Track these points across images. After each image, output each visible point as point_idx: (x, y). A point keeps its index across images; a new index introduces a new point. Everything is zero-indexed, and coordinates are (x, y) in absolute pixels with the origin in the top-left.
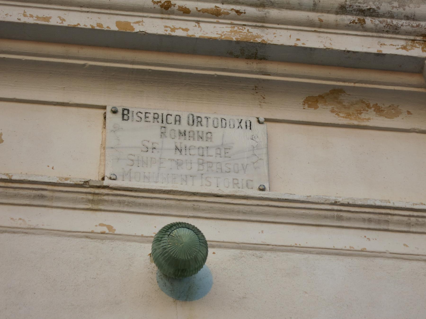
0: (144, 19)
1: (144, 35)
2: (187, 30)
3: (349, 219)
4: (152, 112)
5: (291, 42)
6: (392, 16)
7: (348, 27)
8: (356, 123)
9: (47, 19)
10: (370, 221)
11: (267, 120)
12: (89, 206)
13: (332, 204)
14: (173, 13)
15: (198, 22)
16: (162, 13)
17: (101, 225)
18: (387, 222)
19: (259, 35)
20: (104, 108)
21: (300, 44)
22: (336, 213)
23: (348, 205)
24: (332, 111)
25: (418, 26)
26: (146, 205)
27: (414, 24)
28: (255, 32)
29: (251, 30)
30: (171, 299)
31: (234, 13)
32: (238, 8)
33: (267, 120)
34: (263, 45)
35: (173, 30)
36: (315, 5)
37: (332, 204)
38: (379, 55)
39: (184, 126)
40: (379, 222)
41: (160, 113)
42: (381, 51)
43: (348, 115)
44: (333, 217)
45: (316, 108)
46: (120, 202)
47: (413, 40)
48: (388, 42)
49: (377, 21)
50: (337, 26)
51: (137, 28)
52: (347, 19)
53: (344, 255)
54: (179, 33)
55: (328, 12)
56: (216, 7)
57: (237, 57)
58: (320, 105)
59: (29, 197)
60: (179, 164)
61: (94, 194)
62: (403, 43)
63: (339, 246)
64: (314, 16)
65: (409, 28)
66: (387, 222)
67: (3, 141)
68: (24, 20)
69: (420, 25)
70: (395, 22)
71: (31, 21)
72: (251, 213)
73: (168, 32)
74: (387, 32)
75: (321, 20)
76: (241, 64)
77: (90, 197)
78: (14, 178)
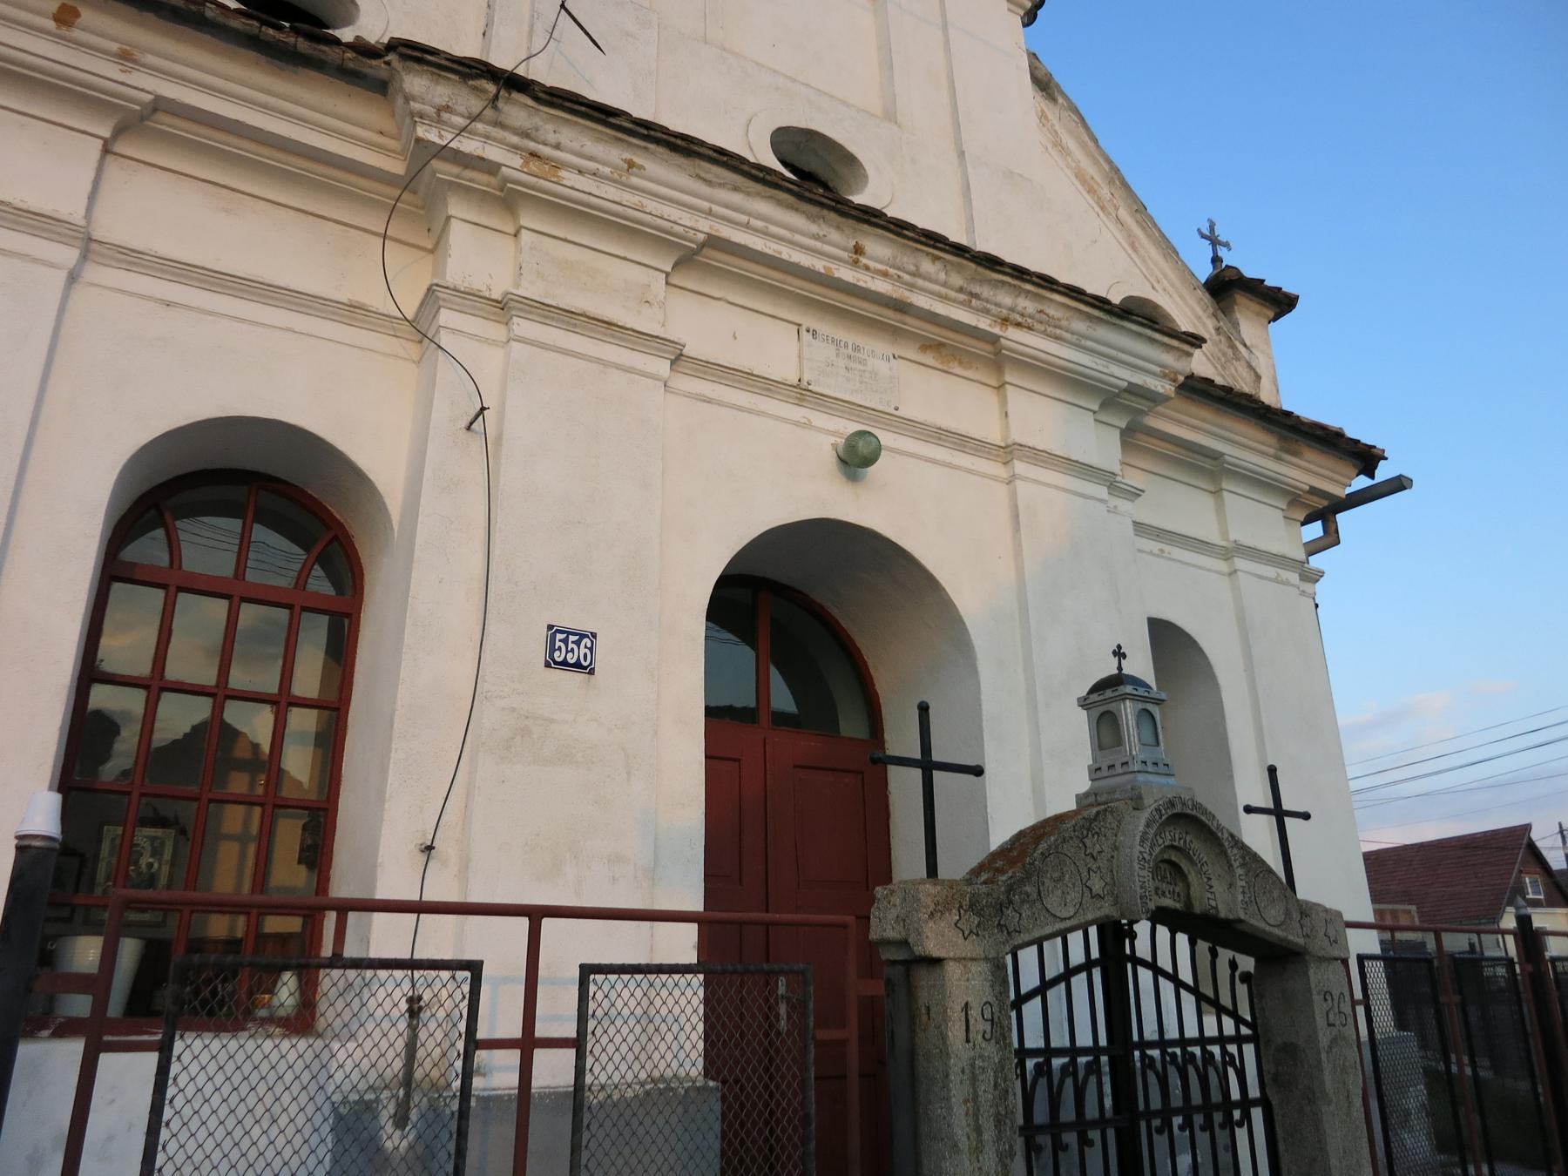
0: (700, 219)
1: (840, 280)
2: (866, 282)
3: (944, 441)
4: (831, 336)
5: (927, 307)
6: (987, 301)
7: (961, 303)
8: (945, 368)
9: (780, 253)
10: (955, 443)
11: (900, 357)
12: (796, 402)
13: (938, 428)
14: (859, 267)
15: (873, 278)
17: (804, 417)
18: (965, 446)
20: (800, 325)
21: (932, 309)
22: (938, 435)
23: (947, 431)
24: (934, 358)
25: (1001, 312)
26: (830, 408)
27: (999, 310)
28: (907, 293)
29: (905, 291)
30: (844, 479)
31: (896, 277)
32: (899, 273)
33: (900, 357)
34: (911, 305)
35: (858, 280)
36: (945, 282)
37: (938, 428)
38: (976, 328)
39: (850, 351)
40: (960, 445)
41: (836, 338)
43: (942, 363)
44: (935, 437)
45: (925, 353)
46: (816, 403)
47: (995, 321)
48: (982, 319)
49: (978, 302)
50: (954, 301)
51: (837, 275)
52: (962, 297)
53: (940, 465)
54: (861, 284)
55: (952, 289)
57: (889, 308)
58: (928, 352)
59: (761, 388)
60: (848, 380)
61: (801, 394)
62: (989, 322)
63: (938, 458)
64: (943, 290)
65: (996, 313)
68: (766, 250)
69: (860, 255)
70: (988, 306)
71: (770, 252)
72: (892, 426)
73: (855, 282)
74: (982, 312)
75: (947, 295)
76: (890, 313)
77: (799, 396)
78: (754, 373)
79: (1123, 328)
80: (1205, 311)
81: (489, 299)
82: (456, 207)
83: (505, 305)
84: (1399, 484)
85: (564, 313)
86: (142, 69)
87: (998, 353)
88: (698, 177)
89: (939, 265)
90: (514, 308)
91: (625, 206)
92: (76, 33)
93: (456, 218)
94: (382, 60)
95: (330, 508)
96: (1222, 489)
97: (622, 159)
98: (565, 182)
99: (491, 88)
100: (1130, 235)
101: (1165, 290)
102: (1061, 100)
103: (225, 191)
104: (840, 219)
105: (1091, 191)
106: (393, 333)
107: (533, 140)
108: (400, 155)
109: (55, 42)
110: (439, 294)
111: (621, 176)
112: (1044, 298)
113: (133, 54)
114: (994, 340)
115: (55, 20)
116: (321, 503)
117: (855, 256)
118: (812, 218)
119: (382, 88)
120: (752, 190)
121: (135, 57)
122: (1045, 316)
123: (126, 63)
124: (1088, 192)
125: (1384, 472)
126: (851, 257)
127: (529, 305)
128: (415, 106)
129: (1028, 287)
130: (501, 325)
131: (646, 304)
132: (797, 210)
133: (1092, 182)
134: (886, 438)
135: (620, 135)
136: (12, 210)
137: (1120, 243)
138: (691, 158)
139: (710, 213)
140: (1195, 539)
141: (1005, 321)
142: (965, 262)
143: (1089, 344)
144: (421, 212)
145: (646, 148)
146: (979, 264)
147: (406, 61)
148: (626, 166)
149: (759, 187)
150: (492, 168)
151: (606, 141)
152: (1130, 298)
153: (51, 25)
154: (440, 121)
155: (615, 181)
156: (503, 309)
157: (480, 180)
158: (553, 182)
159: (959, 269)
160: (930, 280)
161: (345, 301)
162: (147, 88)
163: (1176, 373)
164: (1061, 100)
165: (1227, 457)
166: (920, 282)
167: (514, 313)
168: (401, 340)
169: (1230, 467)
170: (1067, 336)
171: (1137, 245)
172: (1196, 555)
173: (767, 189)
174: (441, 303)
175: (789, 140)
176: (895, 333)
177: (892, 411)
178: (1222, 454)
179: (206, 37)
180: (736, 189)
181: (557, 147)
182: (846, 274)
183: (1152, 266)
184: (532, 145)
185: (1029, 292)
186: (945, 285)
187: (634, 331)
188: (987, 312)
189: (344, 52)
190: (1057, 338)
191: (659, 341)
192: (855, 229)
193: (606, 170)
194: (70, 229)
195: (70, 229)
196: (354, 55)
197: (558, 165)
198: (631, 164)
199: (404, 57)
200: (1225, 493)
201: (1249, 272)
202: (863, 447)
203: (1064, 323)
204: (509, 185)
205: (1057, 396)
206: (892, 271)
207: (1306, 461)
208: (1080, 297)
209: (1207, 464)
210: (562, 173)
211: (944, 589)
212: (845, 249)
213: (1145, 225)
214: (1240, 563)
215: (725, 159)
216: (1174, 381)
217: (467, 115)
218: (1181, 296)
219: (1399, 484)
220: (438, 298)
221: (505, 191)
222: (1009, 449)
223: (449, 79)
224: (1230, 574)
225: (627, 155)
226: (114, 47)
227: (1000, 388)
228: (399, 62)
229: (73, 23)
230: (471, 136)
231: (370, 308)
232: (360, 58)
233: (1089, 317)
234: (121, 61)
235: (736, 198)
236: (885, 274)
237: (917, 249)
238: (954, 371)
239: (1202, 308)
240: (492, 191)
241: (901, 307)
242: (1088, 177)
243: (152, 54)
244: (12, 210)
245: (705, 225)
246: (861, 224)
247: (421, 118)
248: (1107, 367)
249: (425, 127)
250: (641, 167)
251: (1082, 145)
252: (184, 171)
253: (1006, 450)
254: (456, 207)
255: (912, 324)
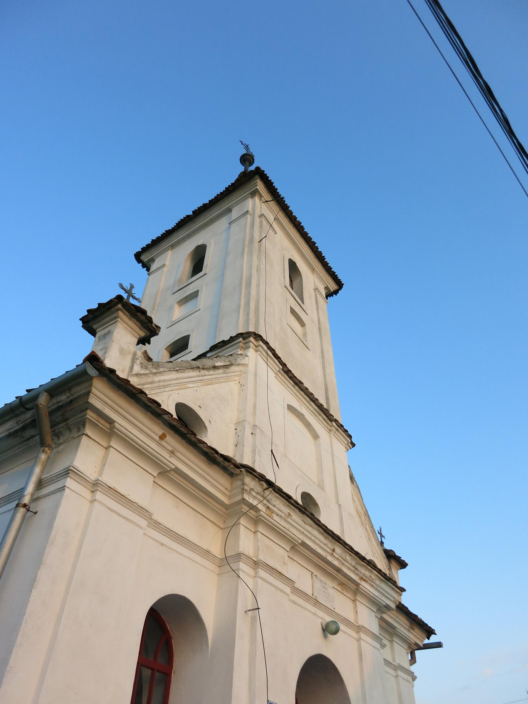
7: (353, 571)
11: (335, 588)
12: (314, 605)
14: (332, 556)
16: (331, 555)
19: (237, 480)
33: (335, 588)
34: (342, 571)
42: (342, 568)
50: (352, 570)
51: (328, 558)
52: (353, 569)
56: (315, 539)
59: (306, 599)
61: (316, 602)
66: (349, 625)
67: (80, 319)
69: (334, 552)
76: (335, 572)
79: (388, 584)
80: (386, 567)
81: (253, 560)
82: (243, 521)
83: (257, 563)
84: (439, 645)
85: (271, 569)
86: (175, 457)
87: (357, 589)
88: (303, 521)
89: (351, 557)
90: (261, 565)
91: (286, 528)
92: (163, 443)
93: (241, 524)
94: (239, 469)
95: (167, 624)
96: (393, 640)
97: (288, 512)
98: (274, 519)
99: (265, 486)
100: (369, 535)
101: (376, 557)
102: (355, 484)
103: (176, 499)
104: (332, 539)
105: (360, 517)
106: (213, 562)
107: (269, 503)
108: (228, 497)
109: (168, 453)
110: (242, 556)
111: (286, 518)
112: (372, 572)
113: (174, 452)
114: (357, 584)
115: (159, 437)
116: (164, 621)
117: (332, 552)
118: (325, 538)
119: (232, 475)
120: (314, 527)
121: (174, 453)
122: (371, 578)
123: (171, 454)
124: (359, 517)
125: (433, 639)
126: (331, 552)
127: (264, 565)
128: (245, 487)
129: (369, 567)
130: (253, 569)
131: (284, 564)
132: (322, 535)
133: (360, 514)
134: (342, 627)
135: (290, 505)
136: (136, 506)
137: (366, 538)
138: (303, 515)
139: (303, 533)
140: (388, 661)
141: (362, 579)
142: (357, 557)
143: (379, 589)
144: (226, 516)
145: (294, 510)
146: (359, 558)
147: (247, 472)
148: (288, 515)
149: (316, 526)
150: (257, 510)
151: (286, 506)
152: (370, 559)
153: (157, 438)
154: (250, 493)
155: (284, 519)
156: (255, 564)
157: (252, 513)
158: (271, 518)
159: (355, 559)
160: (347, 562)
161: (206, 549)
162: (175, 464)
163: (397, 601)
164: (355, 484)
165: (398, 629)
166: (345, 563)
167: (259, 567)
168: (214, 565)
169: (398, 633)
170: (375, 585)
171: (370, 539)
172: (388, 668)
173: (318, 527)
174: (241, 560)
175: (306, 496)
176: (333, 578)
177: (333, 609)
178: (396, 628)
179: (195, 451)
180: (311, 526)
181: (274, 506)
182: (330, 558)
183: (374, 548)
184: (269, 505)
185: (369, 569)
186: (351, 565)
187: (286, 577)
188: (358, 575)
189: (231, 465)
190: (372, 586)
191: (290, 581)
192: (334, 543)
193: (283, 515)
194: (149, 515)
195: (149, 515)
196: (233, 467)
197: (273, 512)
198: (289, 514)
199: (247, 471)
200: (394, 642)
201: (397, 554)
202: (333, 627)
203: (375, 581)
204: (261, 517)
205: (368, 606)
206: (340, 558)
207: (415, 632)
208: (380, 572)
209: (390, 630)
210: (273, 515)
211: (345, 685)
212: (330, 549)
213: (373, 532)
214: (400, 673)
215: (312, 517)
216: (396, 604)
217: (257, 492)
218: (380, 560)
219: (439, 645)
220: (241, 558)
221: (258, 518)
222: (359, 628)
223: (256, 480)
224: (396, 677)
225: (289, 511)
226: (170, 448)
227: (354, 601)
228: (245, 472)
229: (164, 439)
230: (255, 499)
231: (211, 553)
232: (234, 468)
233: (381, 579)
234: (170, 454)
235: (310, 529)
236: (338, 559)
237: (347, 552)
238: (344, 593)
239: (386, 565)
240: (254, 517)
241: (339, 570)
242: (359, 512)
243: (179, 453)
244: (136, 506)
245: (302, 537)
246: (336, 542)
247: (246, 491)
248: (382, 597)
249: (246, 495)
250: (291, 516)
251: (359, 501)
252: (184, 501)
253: (358, 627)
254: (243, 521)
255: (340, 577)
